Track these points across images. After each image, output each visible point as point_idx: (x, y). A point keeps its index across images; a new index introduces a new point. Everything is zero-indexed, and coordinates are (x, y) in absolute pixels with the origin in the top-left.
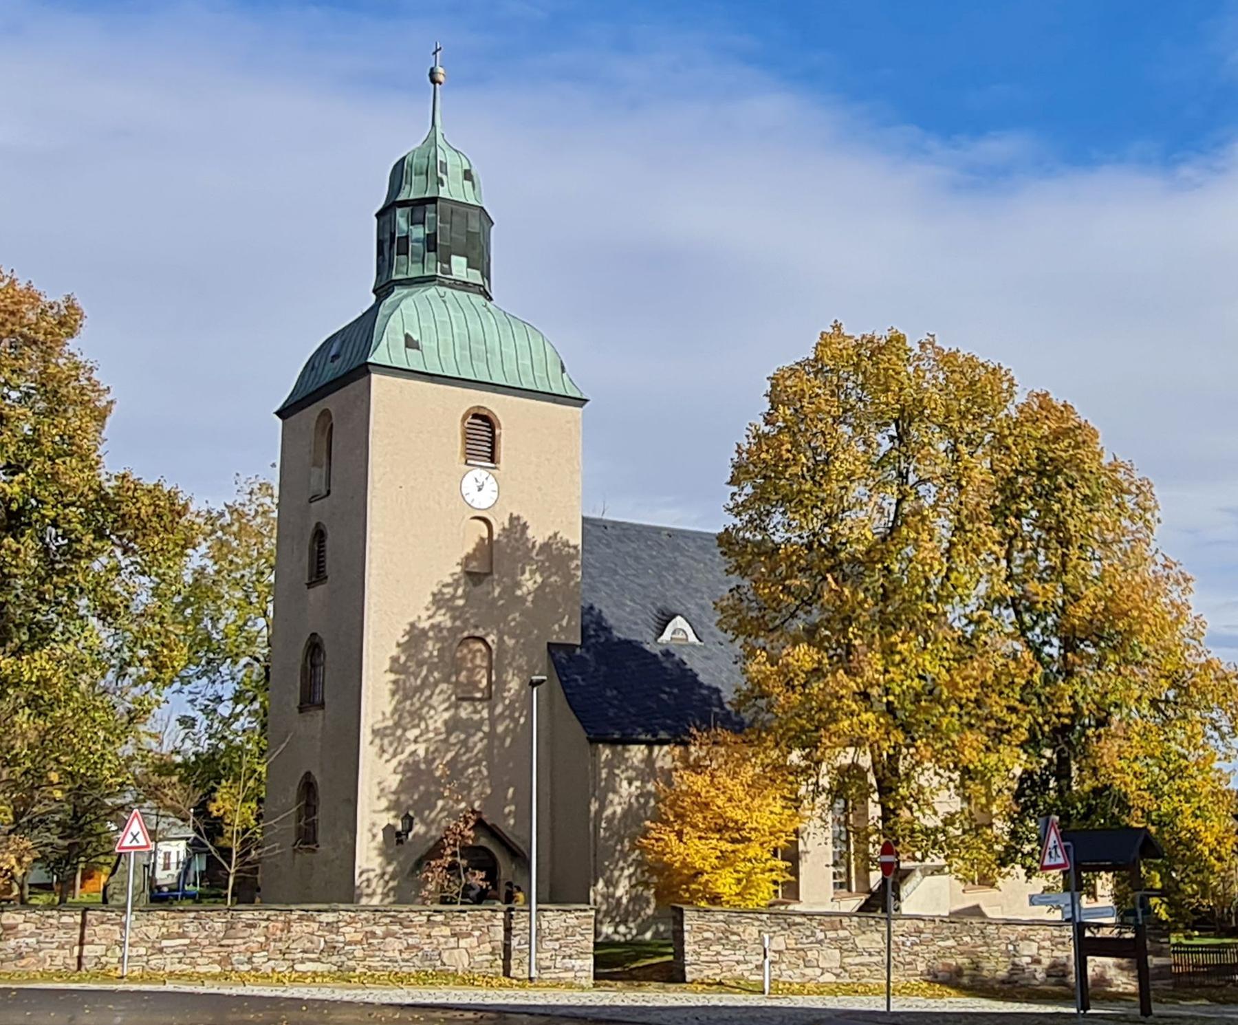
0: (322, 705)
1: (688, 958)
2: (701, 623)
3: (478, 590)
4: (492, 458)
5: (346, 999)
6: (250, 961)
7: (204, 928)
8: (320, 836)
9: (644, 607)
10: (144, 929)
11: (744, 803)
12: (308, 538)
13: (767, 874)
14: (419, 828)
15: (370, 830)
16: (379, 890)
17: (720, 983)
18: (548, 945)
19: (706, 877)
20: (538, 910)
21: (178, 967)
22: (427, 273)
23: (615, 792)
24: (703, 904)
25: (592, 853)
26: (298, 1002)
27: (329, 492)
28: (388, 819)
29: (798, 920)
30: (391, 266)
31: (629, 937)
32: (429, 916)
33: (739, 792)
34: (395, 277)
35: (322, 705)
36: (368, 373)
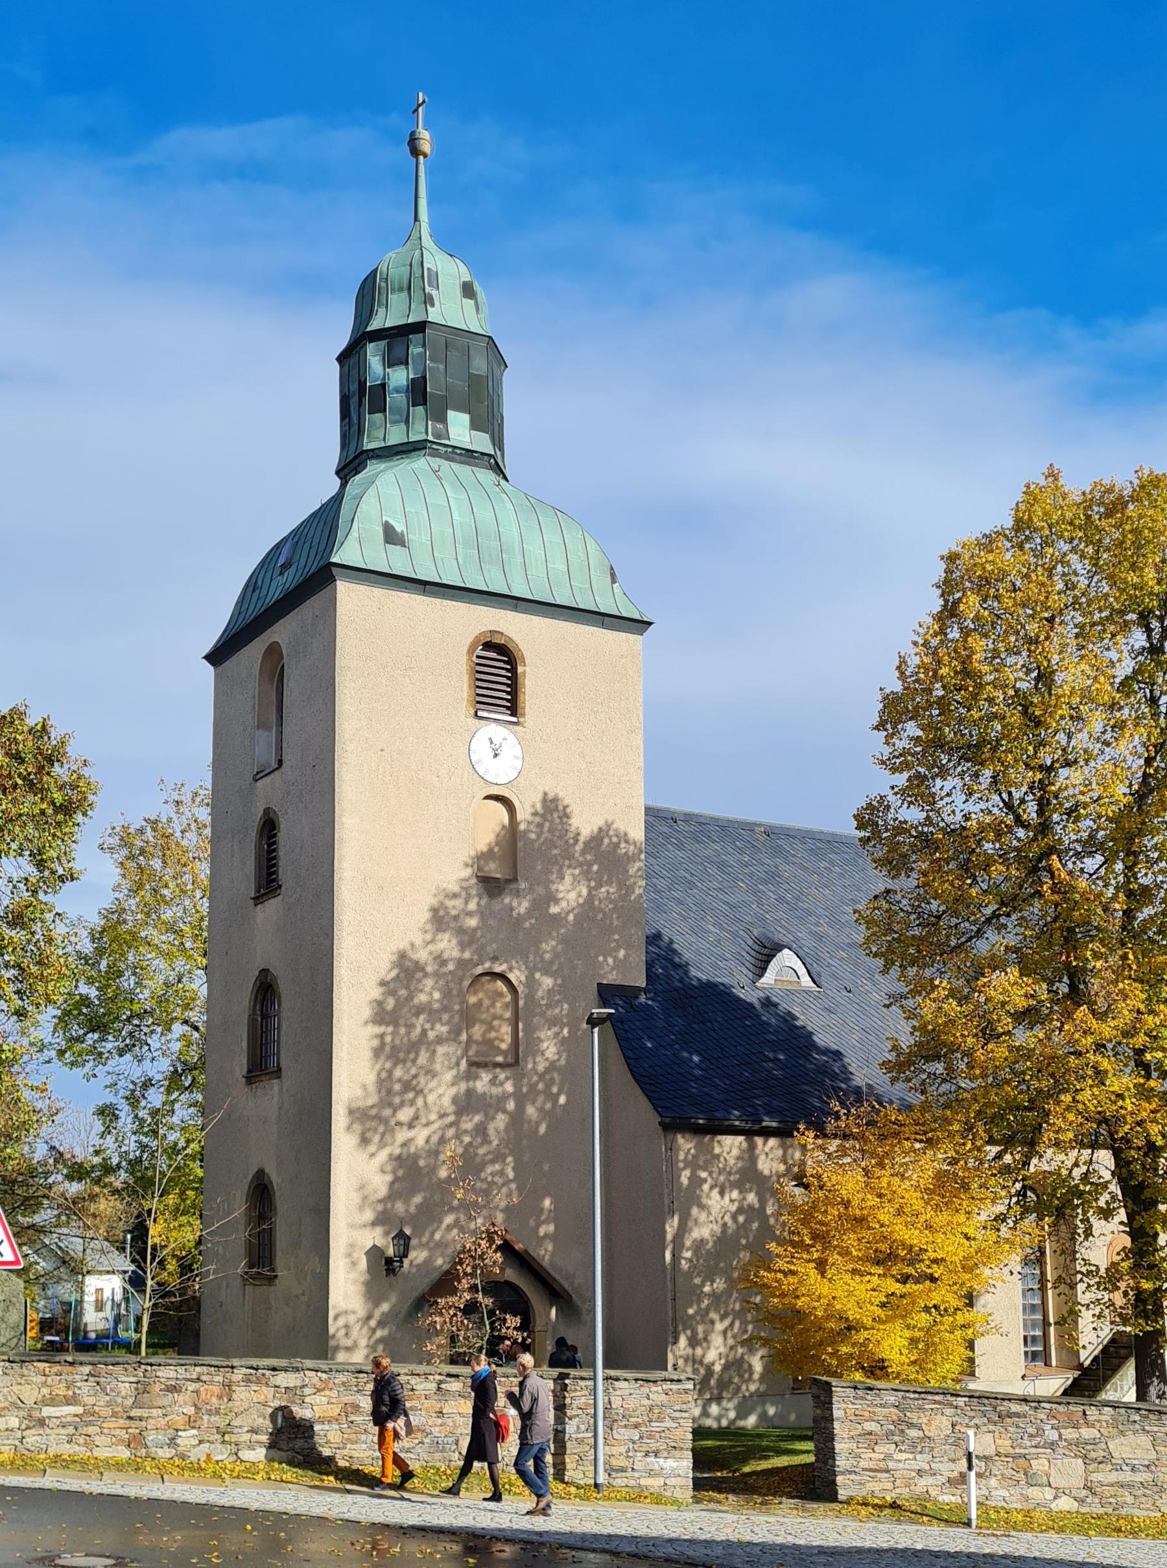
0: (278, 1073)
1: (841, 1463)
2: (818, 960)
3: (497, 905)
4: (513, 708)
5: (317, 1511)
6: (172, 1442)
7: (104, 1390)
8: (280, 1260)
9: (735, 935)
10: (16, 1388)
11: (922, 1218)
12: (253, 834)
13: (958, 1333)
14: (417, 1255)
15: (349, 1255)
16: (363, 1342)
17: (894, 1506)
18: (622, 1434)
19: (864, 1334)
20: (606, 1379)
21: (66, 1450)
22: (413, 438)
23: (702, 1207)
24: (858, 1376)
25: (669, 1296)
26: (241, 1513)
27: (280, 763)
28: (376, 1237)
29: (1015, 1407)
30: (360, 432)
31: (724, 1423)
32: (440, 1382)
33: (914, 1200)
34: (368, 445)
35: (278, 1073)
36: (332, 579)
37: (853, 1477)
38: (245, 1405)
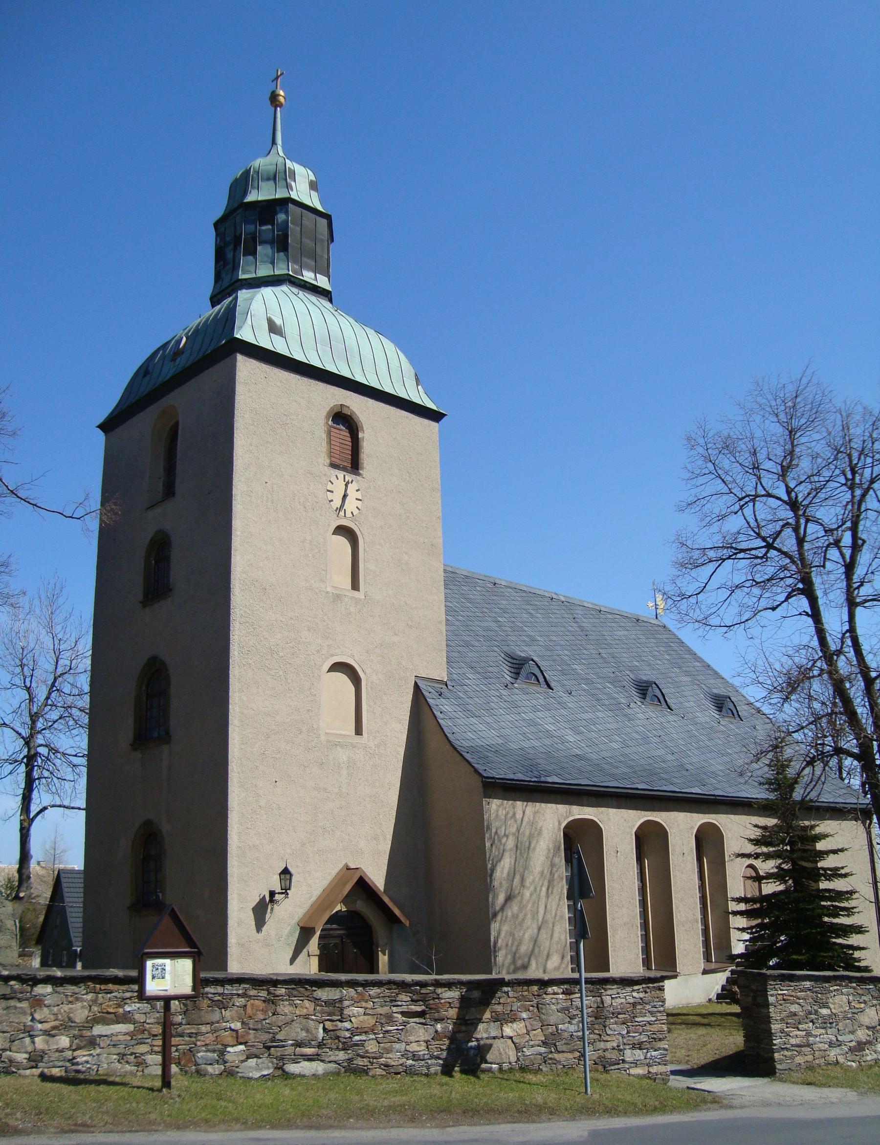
34: (242, 276)
37: (786, 1053)
38: (289, 1018)
